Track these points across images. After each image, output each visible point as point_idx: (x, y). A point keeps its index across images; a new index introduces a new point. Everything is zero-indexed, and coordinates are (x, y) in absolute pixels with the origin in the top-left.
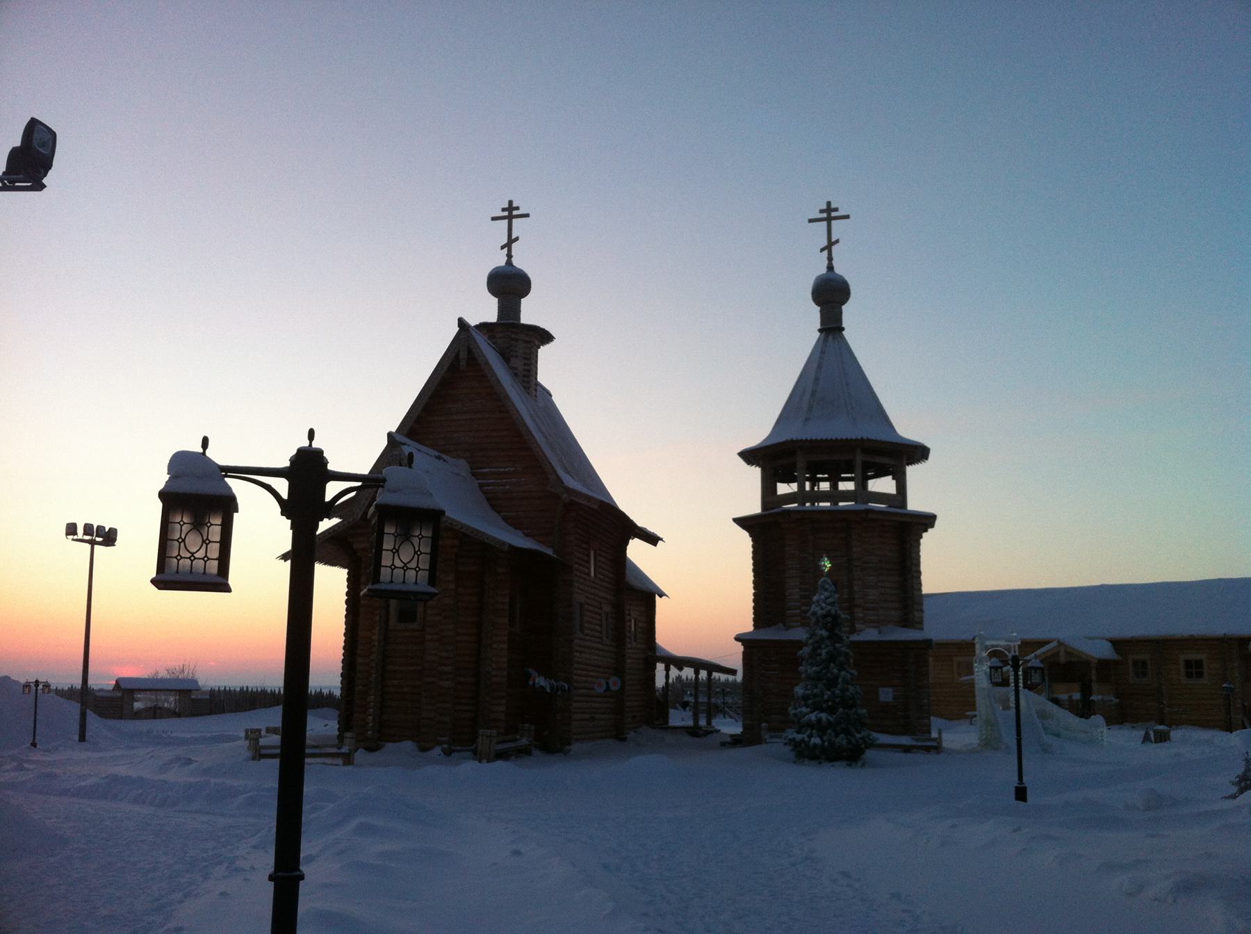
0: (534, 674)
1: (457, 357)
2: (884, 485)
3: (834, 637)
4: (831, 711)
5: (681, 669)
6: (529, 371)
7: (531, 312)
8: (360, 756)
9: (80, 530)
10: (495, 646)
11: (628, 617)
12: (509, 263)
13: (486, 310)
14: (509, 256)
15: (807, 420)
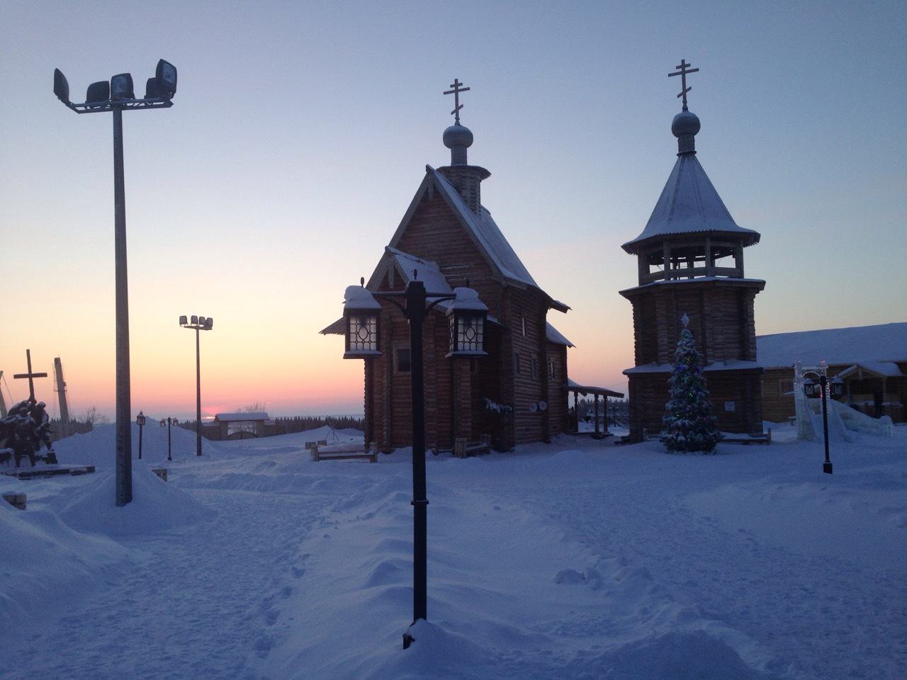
0: (490, 401)
1: (426, 193)
2: (727, 262)
4: (691, 418)
5: (585, 395)
6: (474, 198)
7: (474, 158)
8: (380, 456)
9: (189, 321)
10: (462, 384)
11: (548, 362)
12: (457, 123)
13: (444, 158)
14: (457, 119)
15: (670, 219)
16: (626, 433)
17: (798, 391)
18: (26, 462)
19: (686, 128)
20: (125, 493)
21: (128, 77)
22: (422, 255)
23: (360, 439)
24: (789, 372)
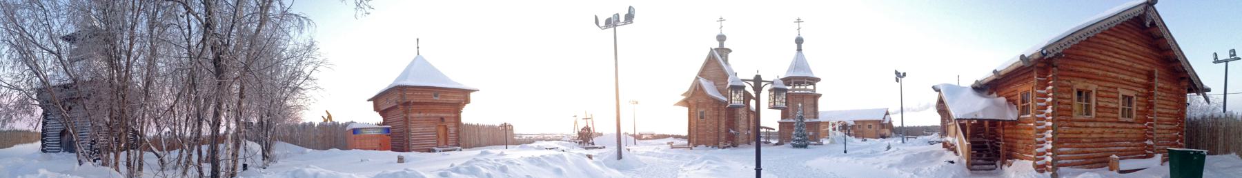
1: (710, 57)
2: (811, 87)
3: (802, 121)
8: (693, 148)
16: (777, 141)
17: (830, 128)
18: (586, 144)
19: (799, 41)
20: (620, 156)
21: (618, 14)
22: (708, 79)
23: (686, 142)
24: (828, 123)
